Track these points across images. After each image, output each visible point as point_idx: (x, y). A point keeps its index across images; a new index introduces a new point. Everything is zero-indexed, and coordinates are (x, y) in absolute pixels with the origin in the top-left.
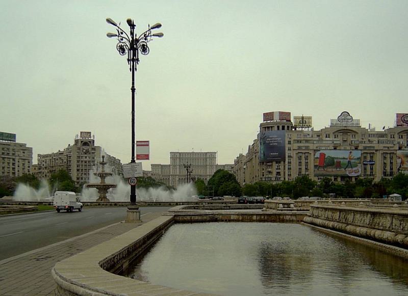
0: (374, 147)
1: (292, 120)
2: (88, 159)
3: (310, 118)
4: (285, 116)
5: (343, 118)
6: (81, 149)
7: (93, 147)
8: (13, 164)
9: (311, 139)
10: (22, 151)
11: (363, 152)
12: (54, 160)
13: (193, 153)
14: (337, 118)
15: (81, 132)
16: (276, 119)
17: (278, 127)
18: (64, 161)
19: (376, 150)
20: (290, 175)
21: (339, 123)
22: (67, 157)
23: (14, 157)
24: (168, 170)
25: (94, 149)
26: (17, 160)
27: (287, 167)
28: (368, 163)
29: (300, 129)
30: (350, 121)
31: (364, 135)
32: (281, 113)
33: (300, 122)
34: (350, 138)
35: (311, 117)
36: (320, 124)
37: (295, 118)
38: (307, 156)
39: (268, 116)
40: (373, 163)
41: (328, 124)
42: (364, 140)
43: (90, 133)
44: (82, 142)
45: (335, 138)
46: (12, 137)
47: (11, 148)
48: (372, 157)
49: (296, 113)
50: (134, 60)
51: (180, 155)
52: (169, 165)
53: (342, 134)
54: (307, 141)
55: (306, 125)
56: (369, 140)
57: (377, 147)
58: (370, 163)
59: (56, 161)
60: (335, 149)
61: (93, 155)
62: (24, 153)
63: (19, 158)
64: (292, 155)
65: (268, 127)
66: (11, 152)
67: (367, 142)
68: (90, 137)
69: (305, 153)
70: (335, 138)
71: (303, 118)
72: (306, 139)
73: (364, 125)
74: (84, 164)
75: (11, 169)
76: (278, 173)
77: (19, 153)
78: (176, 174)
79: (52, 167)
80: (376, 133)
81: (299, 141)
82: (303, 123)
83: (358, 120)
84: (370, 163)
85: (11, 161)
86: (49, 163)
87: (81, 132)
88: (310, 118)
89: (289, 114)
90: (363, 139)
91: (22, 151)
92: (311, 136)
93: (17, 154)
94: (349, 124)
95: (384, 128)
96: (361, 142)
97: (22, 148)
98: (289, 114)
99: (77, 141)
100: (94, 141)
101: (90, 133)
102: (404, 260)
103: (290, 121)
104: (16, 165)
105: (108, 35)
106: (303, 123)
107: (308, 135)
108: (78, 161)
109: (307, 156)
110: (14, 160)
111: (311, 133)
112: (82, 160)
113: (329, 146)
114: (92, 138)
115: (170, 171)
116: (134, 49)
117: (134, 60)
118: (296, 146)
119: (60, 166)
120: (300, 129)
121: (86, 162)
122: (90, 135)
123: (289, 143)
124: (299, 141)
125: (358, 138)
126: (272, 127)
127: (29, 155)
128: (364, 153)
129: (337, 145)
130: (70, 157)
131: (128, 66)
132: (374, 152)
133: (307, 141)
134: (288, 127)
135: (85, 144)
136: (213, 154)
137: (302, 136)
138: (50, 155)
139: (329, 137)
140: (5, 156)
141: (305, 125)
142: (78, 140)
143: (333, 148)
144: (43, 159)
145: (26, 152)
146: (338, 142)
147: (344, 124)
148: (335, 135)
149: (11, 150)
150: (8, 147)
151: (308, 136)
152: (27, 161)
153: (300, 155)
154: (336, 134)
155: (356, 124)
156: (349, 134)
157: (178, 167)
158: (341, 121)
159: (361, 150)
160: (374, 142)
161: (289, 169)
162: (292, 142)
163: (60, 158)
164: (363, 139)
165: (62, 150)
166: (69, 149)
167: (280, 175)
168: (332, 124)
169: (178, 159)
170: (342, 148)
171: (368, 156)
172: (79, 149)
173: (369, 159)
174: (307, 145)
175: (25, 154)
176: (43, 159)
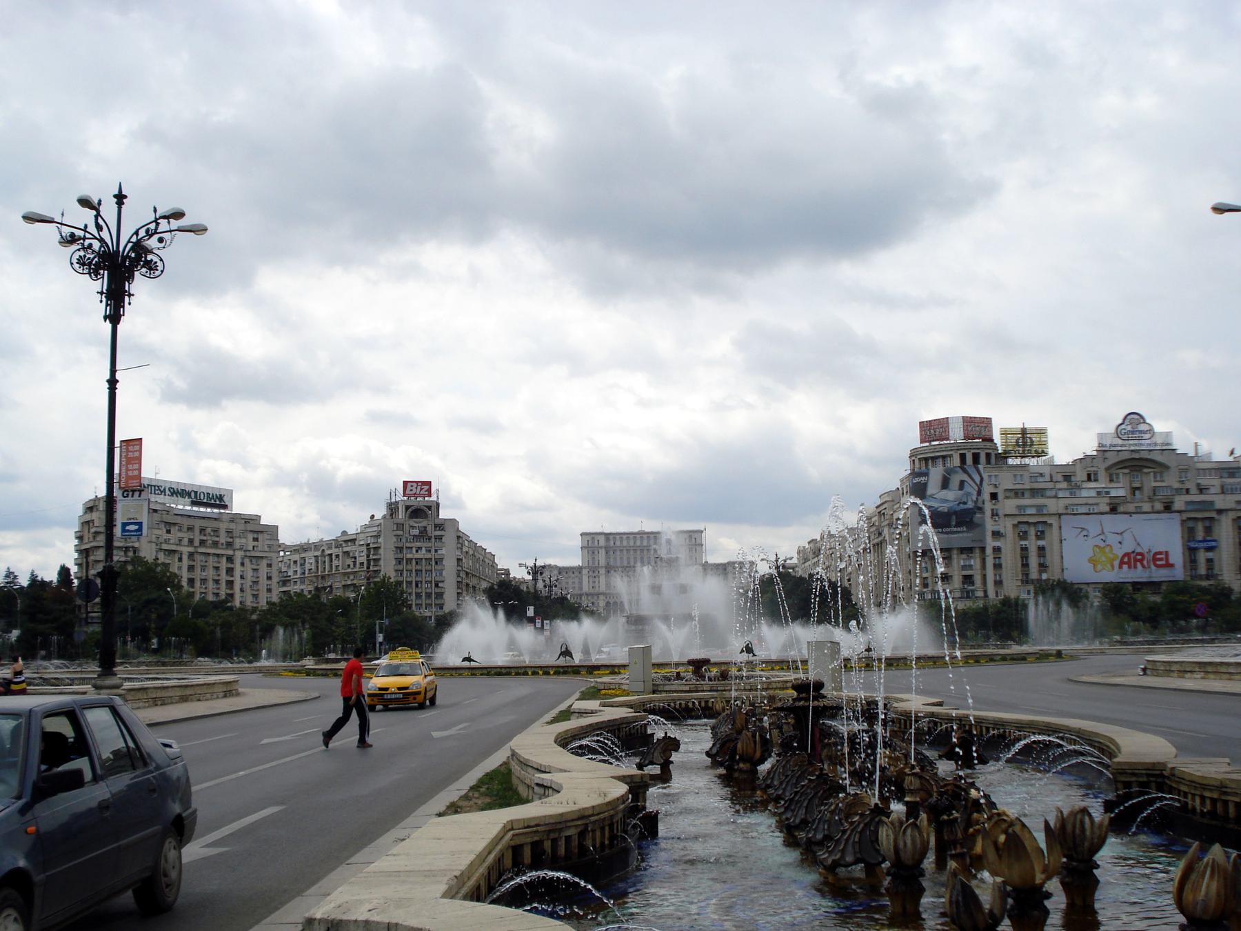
0: (1212, 503)
1: (997, 438)
2: (423, 554)
3: (1042, 432)
4: (978, 427)
5: (1129, 428)
6: (407, 527)
7: (437, 522)
8: (230, 571)
9: (1050, 485)
10: (251, 536)
11: (1185, 516)
12: (327, 559)
13: (642, 533)
14: (1113, 431)
15: (405, 483)
16: (956, 434)
17: (963, 457)
18: (359, 560)
19: (1220, 512)
20: (998, 583)
21: (1120, 442)
22: (368, 550)
23: (230, 552)
24: (577, 581)
25: (440, 526)
26: (238, 561)
27: (990, 562)
28: (1202, 545)
29: (1017, 461)
30: (1147, 436)
31: (1186, 471)
32: (968, 422)
33: (1017, 441)
34: (1150, 482)
35: (1045, 429)
36: (1068, 444)
37: (1005, 433)
38: (1042, 532)
39: (933, 430)
40: (1214, 544)
41: (1089, 447)
42: (1187, 486)
43: (429, 483)
44: (407, 508)
45: (1111, 481)
46: (218, 500)
47: (223, 527)
48: (1208, 530)
49: (1005, 419)
50: (116, 299)
51: (607, 540)
52: (580, 569)
53: (1127, 471)
54: (1035, 492)
55: (1034, 448)
56: (1198, 485)
57: (1221, 502)
58: (1205, 545)
59: (335, 562)
60: (1114, 510)
61: (438, 544)
62: (256, 540)
63: (242, 553)
64: (1002, 531)
65: (934, 459)
66: (223, 539)
67: (1194, 490)
68: (430, 495)
69: (1035, 524)
70: (1111, 481)
71: (1024, 431)
72: (1036, 486)
73: (1183, 444)
74: (414, 566)
75: (223, 585)
76: (968, 579)
77: (244, 541)
78: (596, 590)
79: (323, 577)
80: (1214, 466)
81: (1018, 494)
82: (1025, 445)
83: (1168, 434)
84: (1205, 545)
85: (224, 564)
86: (313, 567)
87: (405, 483)
88: (1042, 432)
89: (987, 422)
90: (1182, 482)
91: (251, 536)
92: (1048, 478)
93: (238, 542)
94: (1145, 444)
95: (1232, 453)
96: (1178, 491)
97: (249, 527)
98: (987, 422)
99: (392, 508)
100: (438, 505)
101: (429, 483)
102: (911, 916)
103: (992, 440)
104: (237, 573)
105: (206, 230)
106: (1025, 445)
107: (1041, 475)
108: (399, 561)
109: (1042, 532)
110: (230, 559)
111: (1047, 471)
112: (409, 556)
113: (1097, 504)
114: (434, 498)
115: (581, 583)
116: (116, 269)
117: (116, 299)
118: (1009, 505)
119: (344, 574)
120: (1017, 461)
121: (418, 561)
122: (429, 490)
123: (994, 496)
124: (1018, 494)
125: (1171, 480)
126: (944, 457)
127: (269, 546)
128: (1189, 519)
129: (1117, 501)
130: (376, 549)
131: (100, 308)
132: (1214, 515)
133: (1035, 492)
134: (988, 455)
135: (416, 513)
136: (695, 535)
137: (1026, 479)
138: (316, 546)
139: (1096, 480)
140: (209, 551)
141: (1030, 451)
142: (397, 502)
143: (1107, 509)
144: (296, 557)
145: (260, 537)
146: (1121, 493)
147: (1132, 444)
148: (1111, 475)
149: (223, 533)
150: (215, 524)
151: (1040, 479)
152: (265, 562)
153: (1024, 528)
154: (1113, 471)
155: (1163, 444)
156: (1146, 470)
157: (603, 571)
158: (1125, 437)
159: (1179, 512)
160: (1212, 490)
161: (998, 566)
162: (1000, 496)
163: (347, 553)
164: (1182, 482)
165: (352, 530)
166: (374, 530)
167: (973, 583)
168: (1100, 445)
169: (603, 552)
170: (1131, 508)
171: (1200, 528)
172: (400, 526)
173: (1200, 534)
174: (1039, 501)
175: (259, 544)
176: (296, 557)
